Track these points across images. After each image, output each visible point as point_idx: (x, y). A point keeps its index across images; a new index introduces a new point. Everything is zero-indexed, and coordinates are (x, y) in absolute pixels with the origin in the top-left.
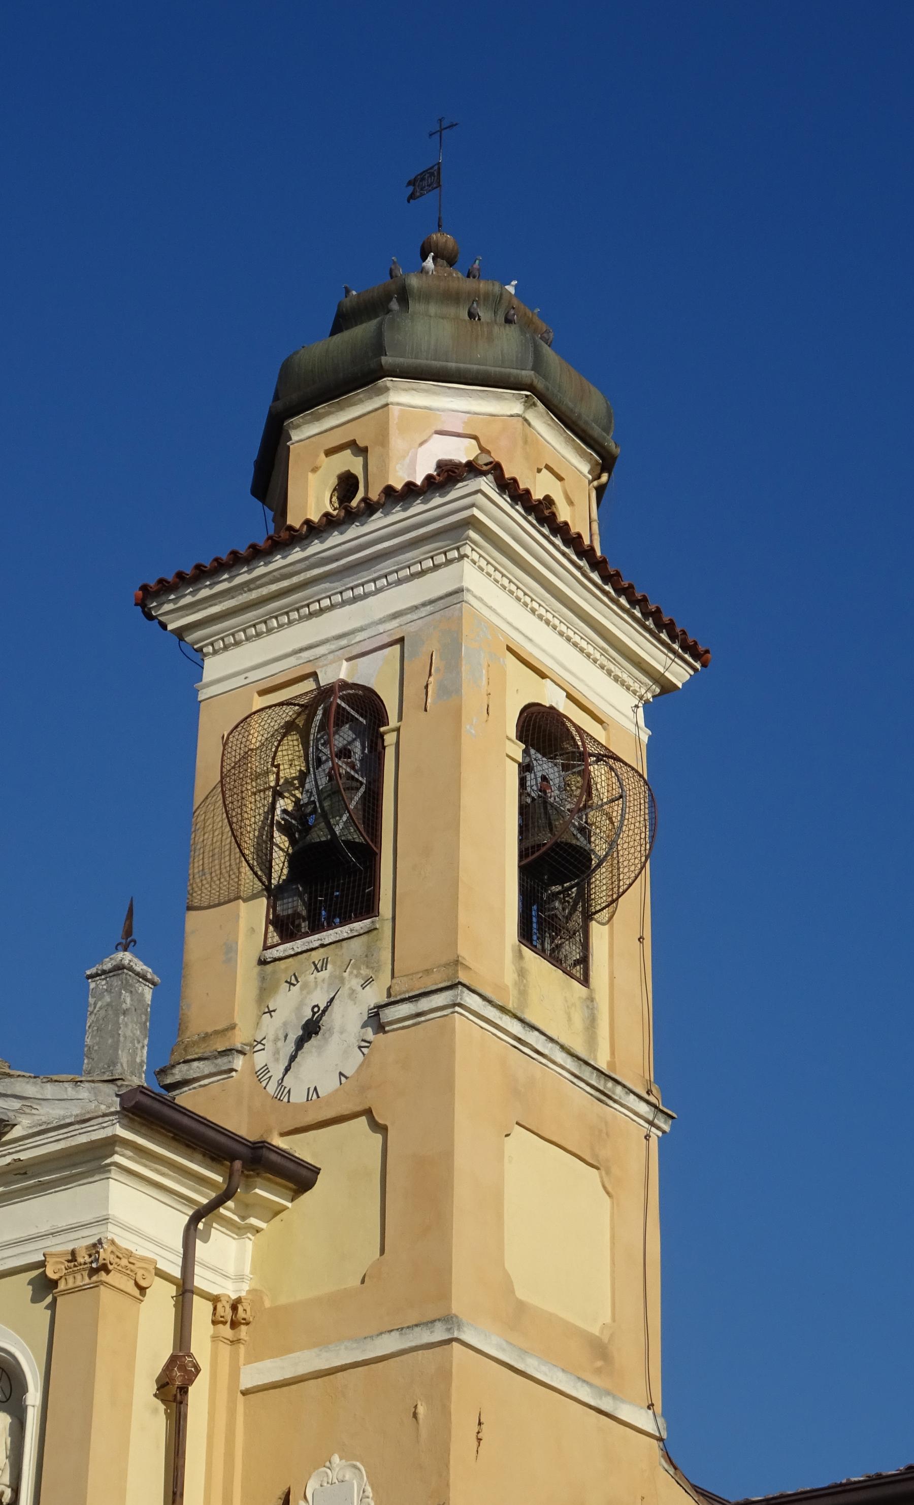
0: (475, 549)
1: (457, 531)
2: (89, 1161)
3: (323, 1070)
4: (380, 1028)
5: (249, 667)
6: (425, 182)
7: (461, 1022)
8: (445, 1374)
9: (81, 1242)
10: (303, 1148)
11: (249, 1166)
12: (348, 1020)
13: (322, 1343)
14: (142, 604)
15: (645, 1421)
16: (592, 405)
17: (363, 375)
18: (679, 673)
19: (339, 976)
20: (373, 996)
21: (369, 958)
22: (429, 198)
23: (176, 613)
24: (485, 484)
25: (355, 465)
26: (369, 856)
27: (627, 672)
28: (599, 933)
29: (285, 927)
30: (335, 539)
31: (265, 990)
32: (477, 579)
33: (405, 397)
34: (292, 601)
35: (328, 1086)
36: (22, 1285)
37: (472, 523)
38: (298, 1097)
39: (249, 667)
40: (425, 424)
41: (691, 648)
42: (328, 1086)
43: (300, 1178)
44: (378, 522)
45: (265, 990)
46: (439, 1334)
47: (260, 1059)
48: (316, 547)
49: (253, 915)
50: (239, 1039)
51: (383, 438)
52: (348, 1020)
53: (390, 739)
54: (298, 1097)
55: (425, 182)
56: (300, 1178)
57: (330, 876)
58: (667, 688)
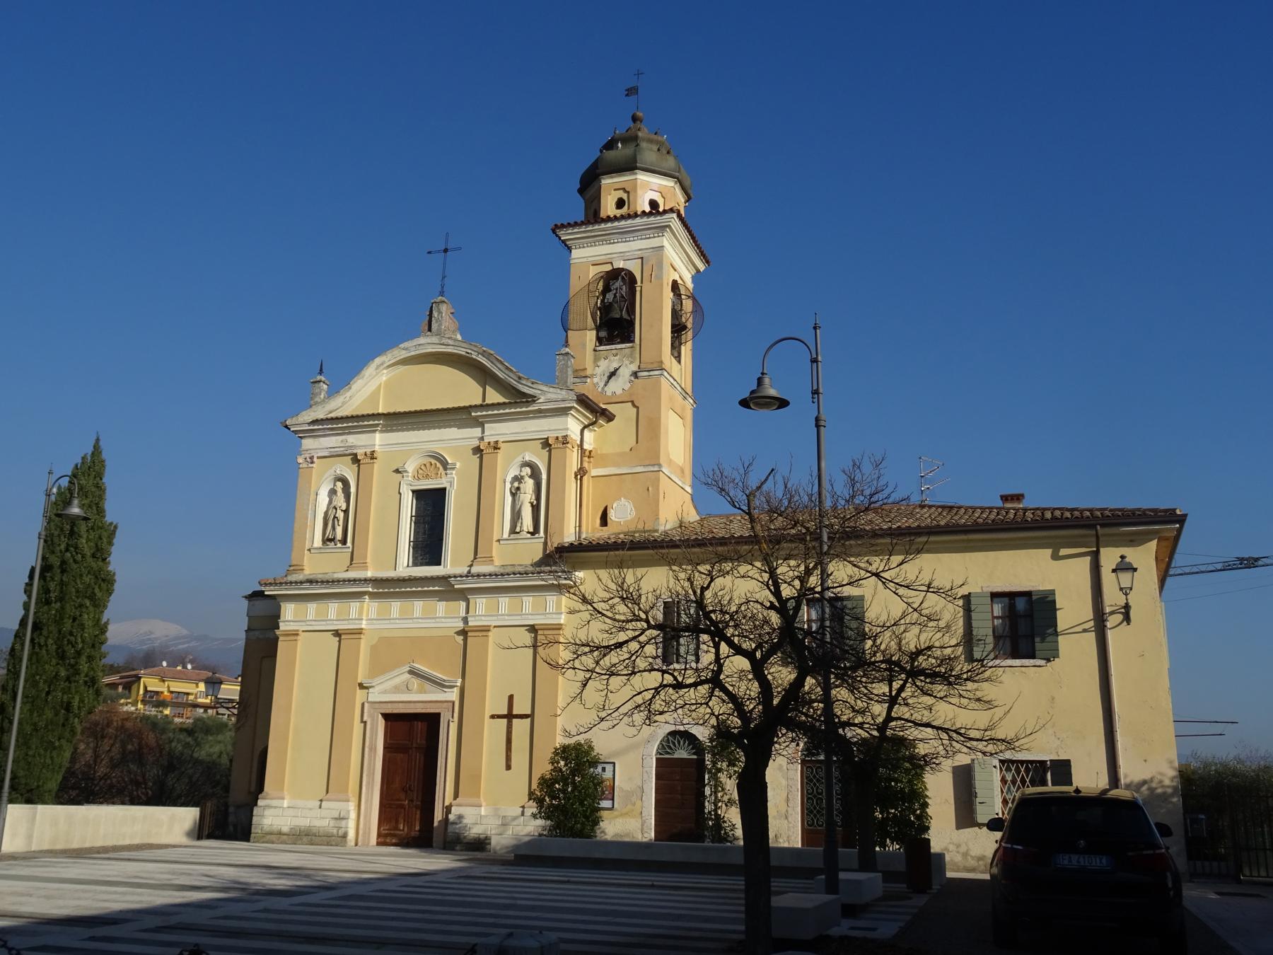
0: (668, 234)
1: (663, 228)
2: (564, 412)
3: (617, 387)
4: (636, 377)
5: (590, 257)
6: (632, 91)
7: (663, 379)
8: (658, 480)
9: (560, 435)
10: (611, 408)
11: (598, 413)
12: (625, 372)
13: (617, 465)
14: (554, 231)
15: (689, 489)
16: (687, 183)
17: (630, 166)
18: (702, 267)
19: (619, 358)
20: (634, 367)
21: (631, 355)
22: (633, 98)
23: (565, 235)
24: (675, 215)
25: (625, 197)
26: (631, 323)
27: (691, 267)
28: (683, 348)
29: (600, 341)
30: (623, 223)
31: (596, 360)
32: (666, 241)
33: (642, 177)
34: (606, 238)
35: (619, 392)
36: (538, 444)
37: (669, 226)
38: (609, 393)
39: (590, 257)
40: (651, 187)
41: (708, 262)
42: (619, 392)
43: (610, 417)
44: (638, 220)
45: (596, 360)
46: (656, 468)
47: (595, 380)
48: (616, 224)
49: (591, 336)
50: (589, 372)
51: (635, 190)
52: (625, 372)
53: (638, 289)
54: (609, 393)
55: (632, 91)
56: (610, 417)
57: (616, 325)
58: (698, 271)
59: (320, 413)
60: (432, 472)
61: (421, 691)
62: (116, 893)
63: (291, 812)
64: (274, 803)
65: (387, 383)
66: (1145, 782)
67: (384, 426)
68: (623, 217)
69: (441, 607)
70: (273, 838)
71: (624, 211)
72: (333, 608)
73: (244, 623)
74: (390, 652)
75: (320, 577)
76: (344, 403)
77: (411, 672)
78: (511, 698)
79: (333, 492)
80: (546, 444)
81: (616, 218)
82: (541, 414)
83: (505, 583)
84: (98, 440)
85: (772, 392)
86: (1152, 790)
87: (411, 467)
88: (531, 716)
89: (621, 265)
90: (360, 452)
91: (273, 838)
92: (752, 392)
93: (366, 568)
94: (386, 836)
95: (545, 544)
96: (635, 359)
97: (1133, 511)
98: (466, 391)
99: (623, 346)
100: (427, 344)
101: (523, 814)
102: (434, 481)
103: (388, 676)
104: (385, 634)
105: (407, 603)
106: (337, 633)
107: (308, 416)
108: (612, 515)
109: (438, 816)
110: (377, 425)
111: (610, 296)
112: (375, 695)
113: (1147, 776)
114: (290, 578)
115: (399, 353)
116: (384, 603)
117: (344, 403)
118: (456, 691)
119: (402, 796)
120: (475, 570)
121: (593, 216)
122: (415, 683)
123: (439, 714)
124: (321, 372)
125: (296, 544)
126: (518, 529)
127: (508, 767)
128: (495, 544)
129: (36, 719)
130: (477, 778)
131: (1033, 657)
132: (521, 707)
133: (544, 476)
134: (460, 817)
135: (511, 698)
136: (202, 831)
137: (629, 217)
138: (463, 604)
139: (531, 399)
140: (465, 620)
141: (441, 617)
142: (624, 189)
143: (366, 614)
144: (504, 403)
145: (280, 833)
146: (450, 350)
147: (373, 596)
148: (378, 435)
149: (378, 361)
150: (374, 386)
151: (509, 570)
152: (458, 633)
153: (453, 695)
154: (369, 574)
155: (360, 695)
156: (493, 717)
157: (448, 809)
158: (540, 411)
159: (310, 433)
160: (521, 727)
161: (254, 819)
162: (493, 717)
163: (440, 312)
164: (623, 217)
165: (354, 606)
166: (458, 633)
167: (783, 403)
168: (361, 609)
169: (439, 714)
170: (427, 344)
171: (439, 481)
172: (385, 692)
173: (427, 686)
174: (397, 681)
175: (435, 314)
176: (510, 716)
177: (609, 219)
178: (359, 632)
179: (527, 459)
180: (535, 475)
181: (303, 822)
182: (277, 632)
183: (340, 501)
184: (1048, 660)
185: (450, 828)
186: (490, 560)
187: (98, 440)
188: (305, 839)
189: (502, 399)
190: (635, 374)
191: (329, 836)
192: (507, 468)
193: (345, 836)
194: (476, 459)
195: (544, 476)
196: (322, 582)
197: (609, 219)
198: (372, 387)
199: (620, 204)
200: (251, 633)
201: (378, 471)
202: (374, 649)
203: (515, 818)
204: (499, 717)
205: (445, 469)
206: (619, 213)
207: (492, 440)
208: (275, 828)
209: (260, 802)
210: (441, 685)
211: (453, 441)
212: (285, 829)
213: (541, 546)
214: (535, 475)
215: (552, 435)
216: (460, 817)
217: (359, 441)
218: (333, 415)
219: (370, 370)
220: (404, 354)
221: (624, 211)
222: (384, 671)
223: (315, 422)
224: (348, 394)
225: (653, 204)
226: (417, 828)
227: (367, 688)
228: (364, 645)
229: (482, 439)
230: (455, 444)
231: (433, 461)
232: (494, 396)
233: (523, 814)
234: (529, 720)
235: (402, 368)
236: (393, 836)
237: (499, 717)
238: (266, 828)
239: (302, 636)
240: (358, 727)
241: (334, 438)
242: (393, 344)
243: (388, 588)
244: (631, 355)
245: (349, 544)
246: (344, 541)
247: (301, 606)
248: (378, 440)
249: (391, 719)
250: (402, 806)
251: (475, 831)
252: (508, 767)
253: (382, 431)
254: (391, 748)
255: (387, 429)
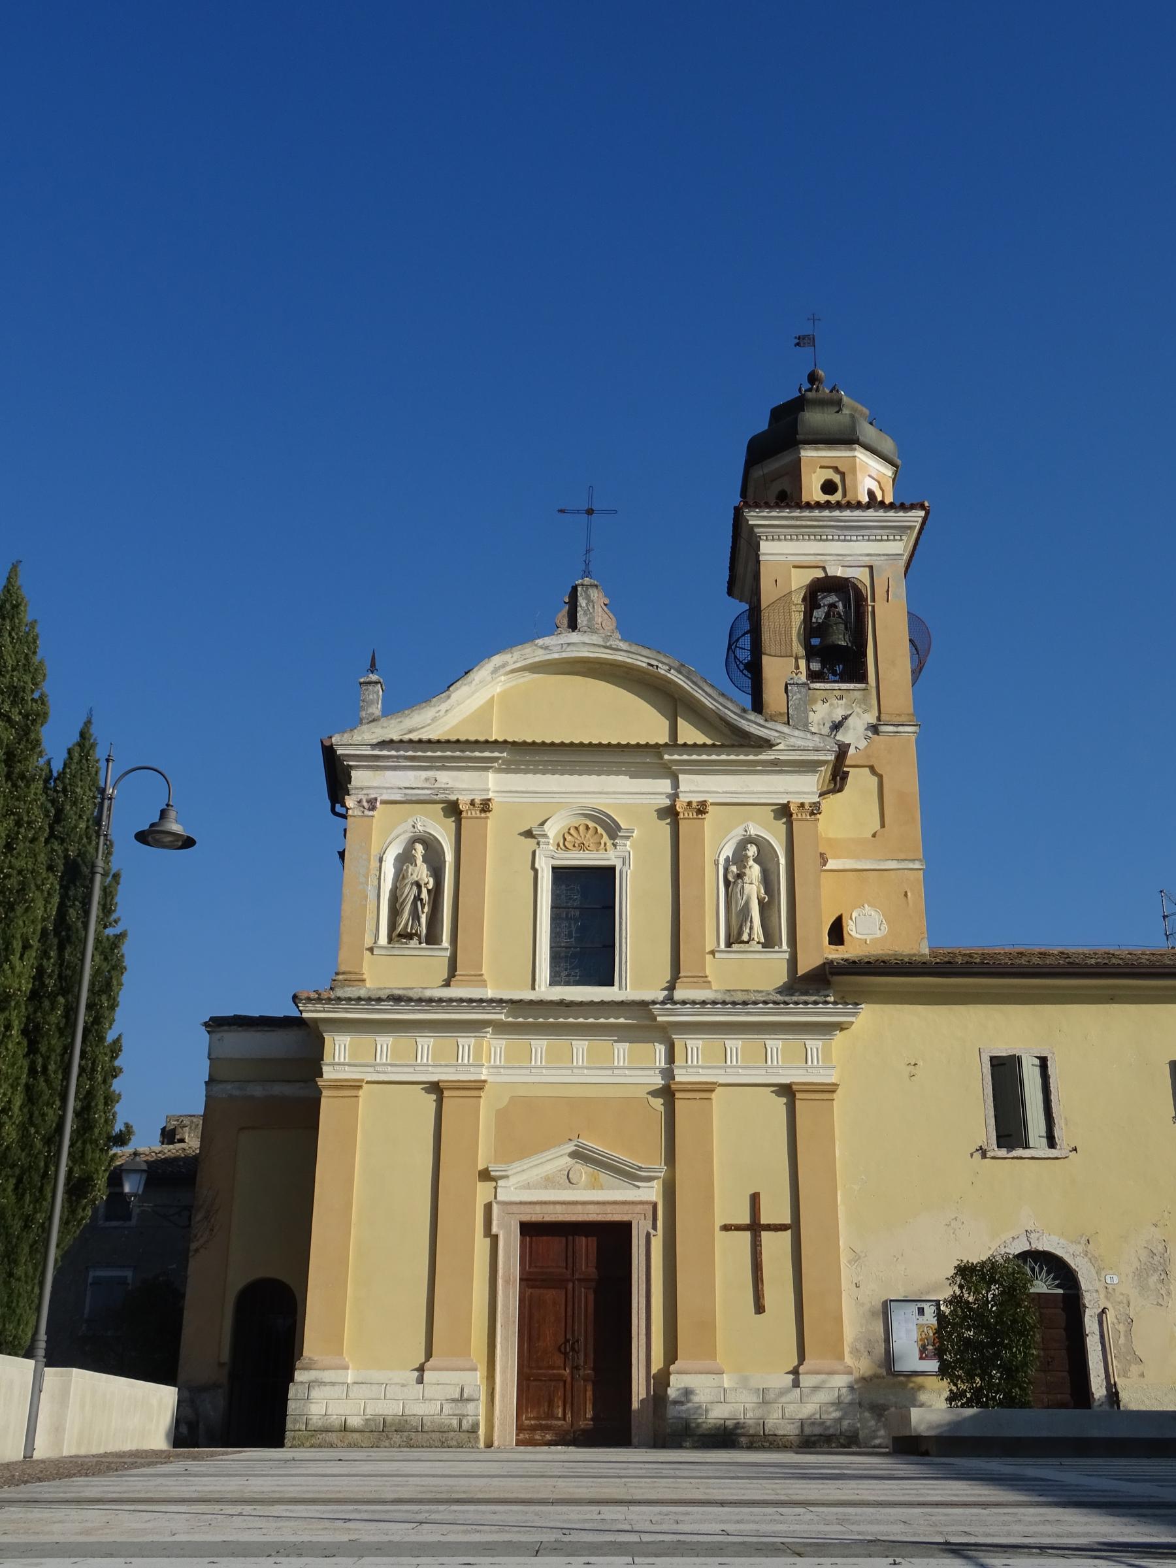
13: (856, 857)
22: (808, 350)
25: (837, 479)
34: (817, 533)
39: (790, 557)
48: (837, 513)
59: (393, 730)
60: (589, 840)
61: (594, 1185)
62: (399, 1511)
63: (364, 1391)
64: (328, 1376)
65: (504, 695)
67: (505, 762)
68: (828, 505)
69: (622, 1051)
70: (332, 1437)
75: (414, 994)
76: (434, 719)
77: (574, 1155)
78: (755, 1199)
79: (405, 858)
80: (784, 812)
81: (819, 506)
82: (777, 767)
83: (734, 1017)
84: (88, 723)
85: (176, 828)
87: (553, 830)
88: (794, 1227)
89: (839, 572)
90: (463, 800)
91: (332, 1437)
92: (152, 825)
94: (533, 1429)
95: (793, 962)
96: (871, 706)
98: (645, 723)
99: (851, 686)
102: (594, 855)
103: (535, 1160)
105: (560, 1043)
106: (435, 1088)
107: (370, 734)
109: (639, 1390)
110: (496, 759)
111: (819, 615)
112: (509, 1191)
114: (340, 993)
115: (533, 653)
116: (518, 1042)
117: (434, 719)
119: (558, 1360)
120: (679, 995)
121: (788, 496)
122: (583, 1172)
123: (628, 1225)
124: (373, 668)
125: (346, 939)
126: (745, 937)
127: (760, 1308)
128: (709, 957)
129: (28, 1209)
130: (707, 1326)
132: (775, 1210)
134: (688, 1392)
135: (755, 1199)
136: (189, 1433)
137: (839, 506)
138: (661, 1049)
139: (766, 744)
140: (668, 1074)
141: (632, 1068)
142: (836, 470)
143: (488, 1058)
144: (704, 745)
147: (500, 1028)
149: (497, 660)
150: (485, 697)
151: (739, 997)
153: (652, 1192)
154: (490, 993)
155: (483, 1191)
156: (726, 1228)
158: (775, 763)
159: (373, 762)
160: (776, 1246)
161: (292, 1406)
162: (726, 1228)
163: (589, 600)
164: (828, 505)
165: (467, 1042)
166: (655, 1093)
167: (189, 843)
169: (628, 1225)
171: (601, 854)
172: (528, 1186)
173: (604, 1177)
175: (582, 602)
176: (755, 1227)
177: (808, 506)
178: (479, 1086)
179: (753, 830)
180: (765, 858)
181: (390, 1409)
182: (320, 1083)
183: (421, 872)
185: (672, 1411)
186: (703, 981)
187: (88, 723)
188: (396, 1438)
189: (701, 739)
190: (874, 729)
191: (443, 1430)
192: (717, 843)
193: (474, 1430)
194: (664, 827)
197: (808, 506)
199: (829, 487)
200: (217, 1088)
202: (503, 1117)
203: (783, 1392)
204: (738, 1228)
206: (823, 498)
207: (696, 798)
209: (299, 1376)
210: (630, 1176)
211: (631, 795)
212: (355, 1422)
213: (784, 966)
214: (765, 858)
215: (795, 800)
216: (688, 1392)
217: (462, 783)
218: (414, 736)
219: (482, 673)
220: (540, 656)
223: (383, 744)
224: (444, 707)
225: (871, 494)
226: (589, 1415)
227: (495, 1179)
228: (486, 1107)
229: (674, 796)
231: (591, 824)
232: (689, 733)
233: (796, 1384)
234: (788, 1234)
235: (529, 677)
236: (547, 1428)
237: (738, 1228)
238: (316, 1422)
239: (365, 1086)
240: (481, 1245)
241: (411, 774)
242: (527, 637)
243: (528, 1018)
244: (865, 700)
246: (432, 938)
247: (366, 1040)
248: (494, 783)
249: (529, 1229)
250: (560, 1379)
251: (718, 1414)
252: (760, 1308)
253: (499, 771)
254: (533, 1280)
255: (509, 768)
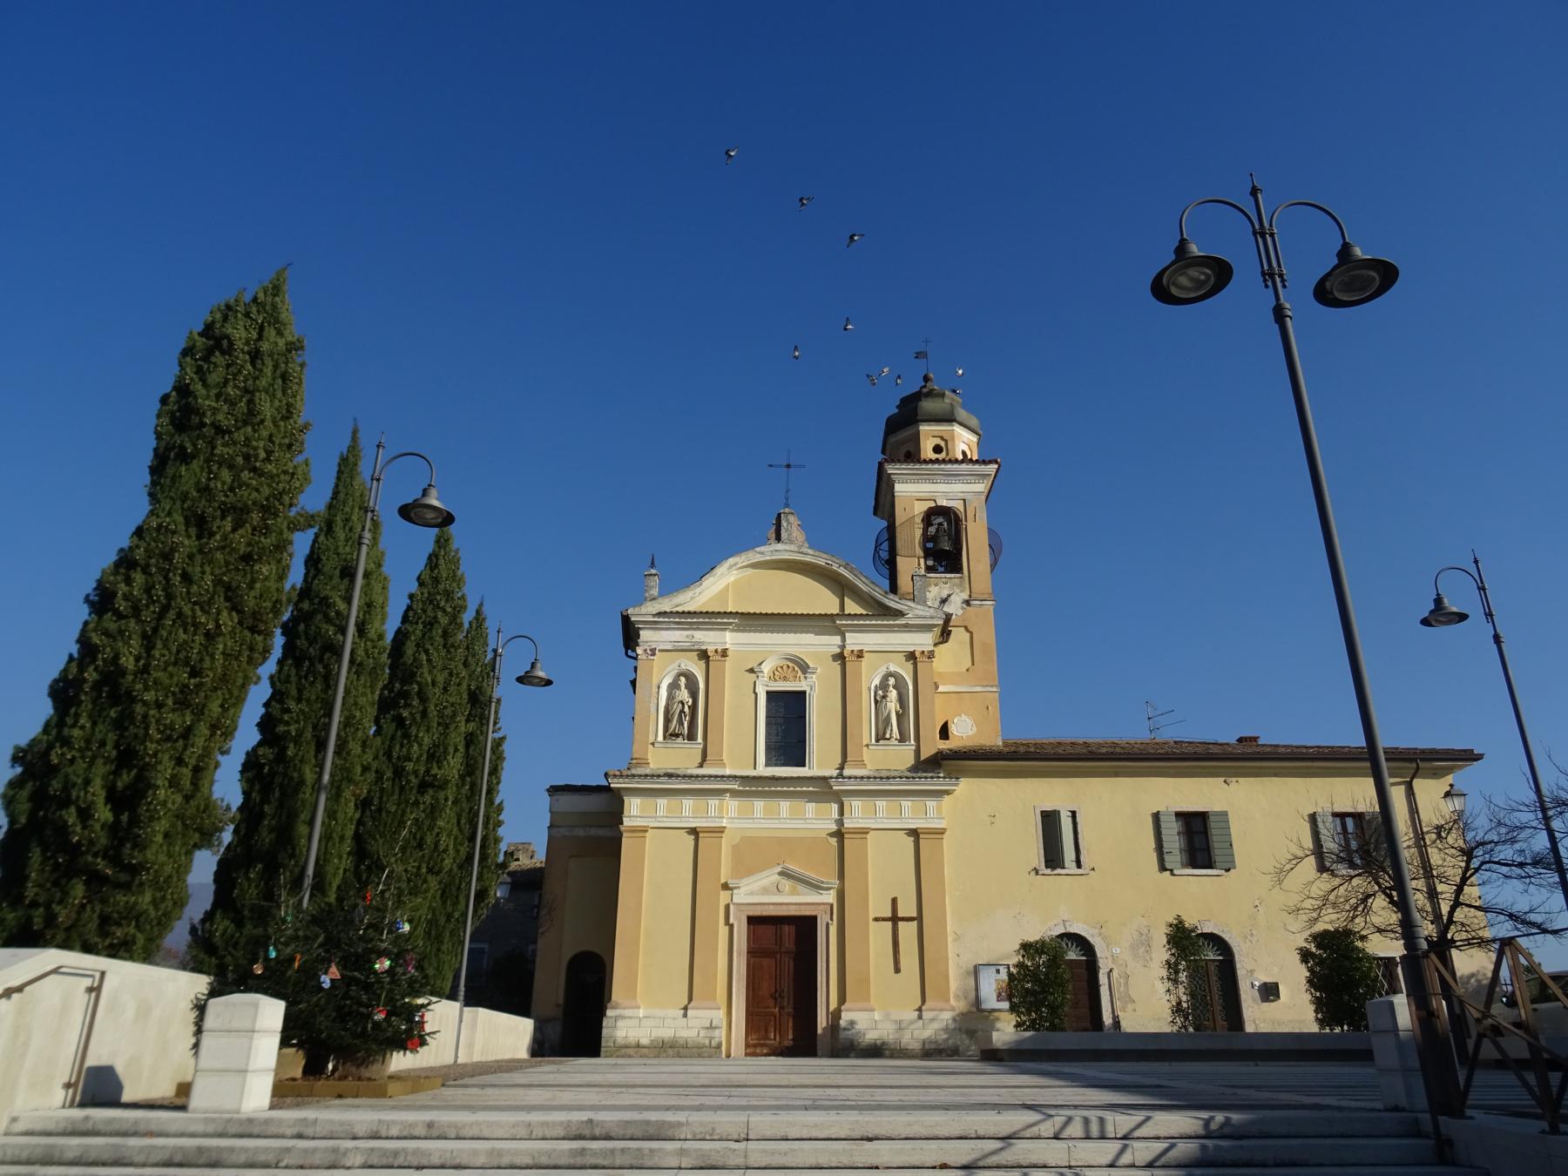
17: (949, 419)
25: (943, 444)
33: (957, 429)
34: (930, 478)
36: (902, 657)
39: (914, 493)
60: (790, 675)
61: (793, 892)
64: (627, 1013)
66: (1473, 975)
68: (937, 461)
71: (942, 456)
72: (688, 803)
73: (546, 820)
74: (753, 854)
77: (780, 874)
78: (894, 901)
80: (911, 656)
81: (931, 461)
82: (908, 628)
83: (881, 787)
86: (1478, 981)
88: (919, 918)
89: (945, 503)
90: (711, 649)
93: (723, 765)
94: (755, 1046)
95: (918, 752)
97: (1423, 751)
98: (823, 600)
100: (782, 551)
101: (920, 1017)
104: (748, 834)
105: (772, 803)
106: (694, 832)
108: (953, 729)
109: (822, 1022)
112: (740, 896)
113: (1474, 970)
114: (634, 771)
115: (753, 556)
118: (833, 893)
119: (771, 1002)
120: (846, 772)
121: (912, 456)
122: (787, 884)
123: (815, 918)
124: (653, 565)
125: (637, 736)
127: (897, 970)
130: (865, 981)
131: (1210, 867)
132: (907, 908)
133: (702, 685)
134: (852, 1023)
135: (894, 901)
136: (541, 1048)
137: (944, 461)
138: (835, 807)
139: (900, 614)
140: (840, 822)
141: (816, 819)
145: (638, 1046)
146: (808, 559)
147: (734, 793)
148: (728, 634)
149: (731, 561)
150: (724, 584)
151: (884, 774)
152: (831, 835)
153: (830, 897)
154: (728, 772)
155: (724, 897)
156: (876, 919)
157: (836, 1015)
158: (906, 626)
159: (653, 625)
160: (908, 931)
161: (605, 1032)
162: (876, 919)
164: (937, 461)
165: (713, 802)
166: (831, 835)
168: (721, 806)
169: (815, 918)
170: (782, 551)
172: (752, 893)
173: (800, 887)
174: (765, 882)
175: (784, 523)
176: (895, 919)
177: (925, 462)
178: (721, 830)
179: (892, 668)
181: (666, 1033)
183: (684, 694)
184: (1228, 870)
185: (843, 1035)
187: (481, 605)
188: (670, 1052)
189: (859, 610)
190: (967, 602)
191: (700, 1047)
192: (870, 676)
194: (837, 666)
195: (702, 685)
196: (684, 776)
197: (925, 462)
198: (721, 585)
199: (937, 449)
200: (555, 830)
201: (730, 672)
202: (736, 849)
203: (912, 1022)
204: (884, 919)
205: (804, 672)
206: (934, 456)
207: (856, 648)
208: (632, 1040)
209: (609, 1013)
210: (816, 887)
211: (816, 646)
214: (900, 686)
215: (919, 649)
217: (709, 639)
218: (680, 609)
220: (759, 558)
221: (942, 456)
222: (751, 872)
223: (660, 614)
224: (698, 590)
228: (726, 843)
230: (812, 649)
232: (852, 607)
235: (751, 571)
236: (762, 1045)
237: (884, 919)
238: (620, 1041)
240: (723, 931)
241: (678, 633)
243: (752, 787)
244: (961, 585)
245: (700, 740)
246: (691, 737)
247: (650, 801)
248: (729, 639)
252: (897, 970)
254: (753, 952)
